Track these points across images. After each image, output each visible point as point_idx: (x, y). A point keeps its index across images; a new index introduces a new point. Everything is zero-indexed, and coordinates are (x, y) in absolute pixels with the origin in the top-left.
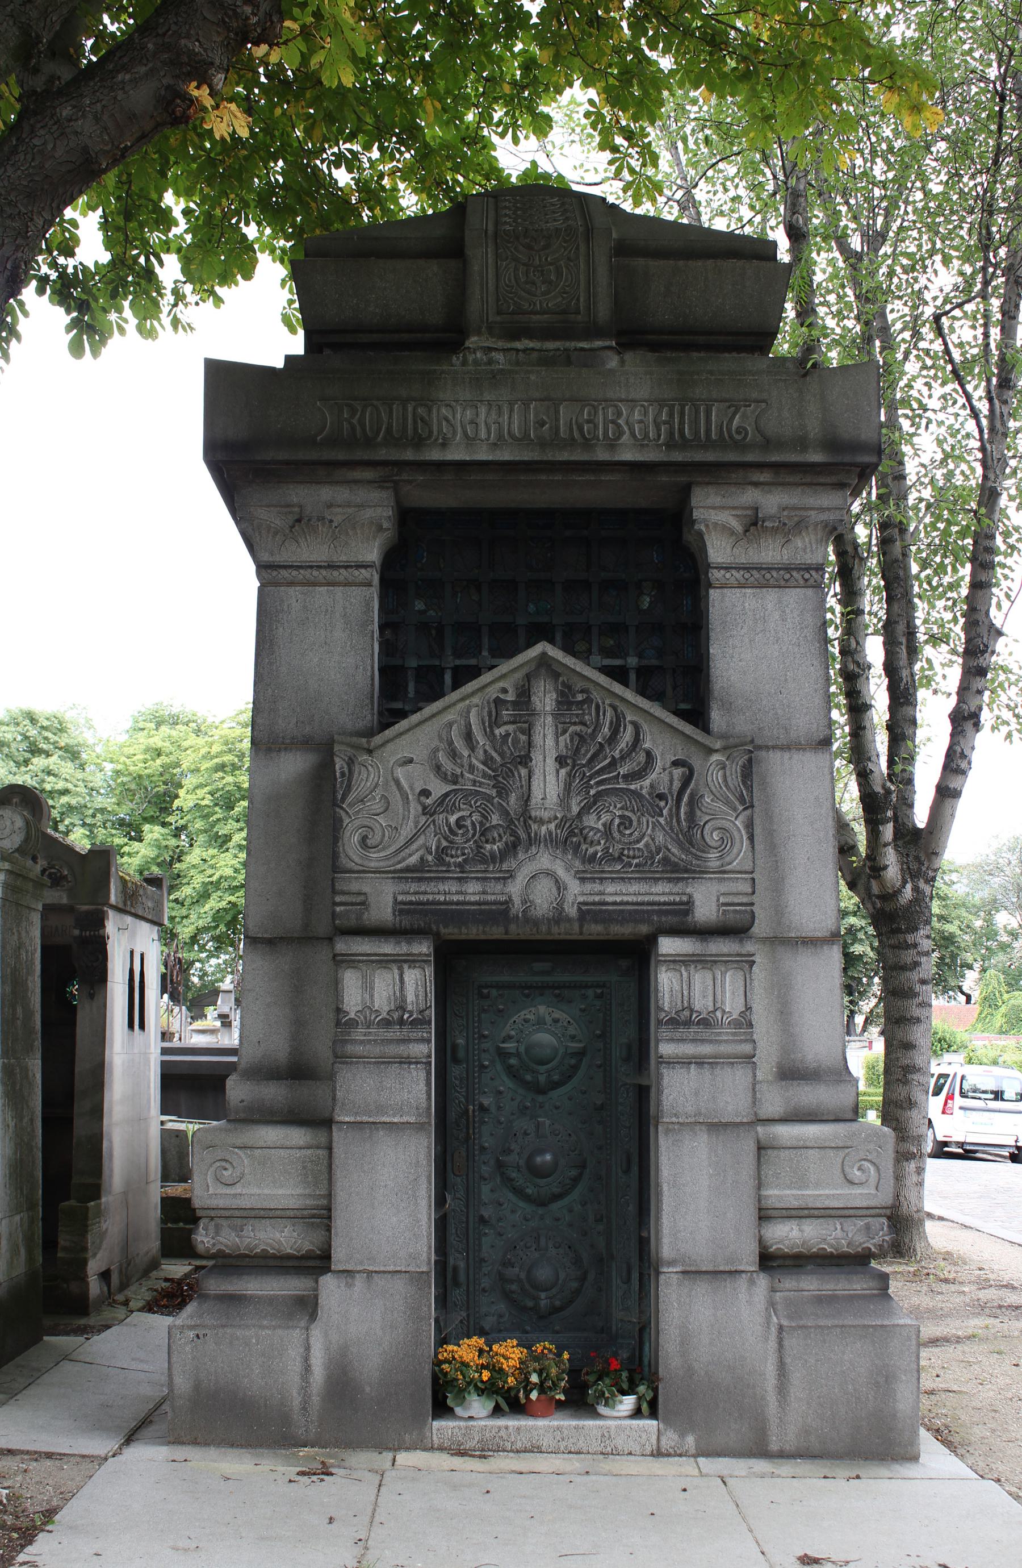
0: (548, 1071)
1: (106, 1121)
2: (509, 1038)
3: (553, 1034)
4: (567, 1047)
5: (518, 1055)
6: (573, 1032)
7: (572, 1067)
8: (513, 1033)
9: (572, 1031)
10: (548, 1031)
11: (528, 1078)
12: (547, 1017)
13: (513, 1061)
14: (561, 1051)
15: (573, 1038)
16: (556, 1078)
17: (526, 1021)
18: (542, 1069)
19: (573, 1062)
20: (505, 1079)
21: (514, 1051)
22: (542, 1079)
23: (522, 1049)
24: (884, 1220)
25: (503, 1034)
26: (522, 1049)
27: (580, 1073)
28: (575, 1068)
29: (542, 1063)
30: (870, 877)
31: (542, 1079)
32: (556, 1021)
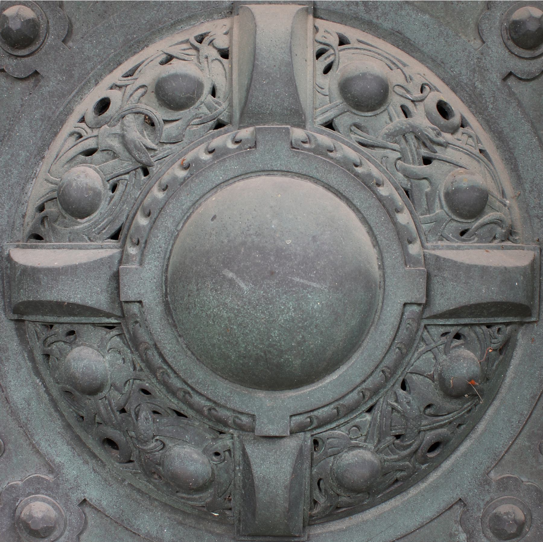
0: (309, 424)
1: (287, 391)
2: (72, 207)
3: (351, 184)
4: (432, 273)
5: (119, 319)
6: (473, 176)
7: (454, 393)
8: (88, 177)
9: (465, 165)
10: (314, 163)
11: (189, 458)
12: (308, 72)
13: (92, 357)
14: (400, 292)
15: (469, 208)
16: (359, 459)
17: (173, 97)
18: (272, 409)
19: (464, 362)
20: (61, 452)
21: (95, 295)
22: (274, 468)
23: (143, 283)
24: (53, 525)
25: (38, 190)
26: (143, 283)
27: (497, 423)
28: (470, 396)
29: (274, 376)
30: (257, 232)
31: (274, 468)
32: (364, 98)
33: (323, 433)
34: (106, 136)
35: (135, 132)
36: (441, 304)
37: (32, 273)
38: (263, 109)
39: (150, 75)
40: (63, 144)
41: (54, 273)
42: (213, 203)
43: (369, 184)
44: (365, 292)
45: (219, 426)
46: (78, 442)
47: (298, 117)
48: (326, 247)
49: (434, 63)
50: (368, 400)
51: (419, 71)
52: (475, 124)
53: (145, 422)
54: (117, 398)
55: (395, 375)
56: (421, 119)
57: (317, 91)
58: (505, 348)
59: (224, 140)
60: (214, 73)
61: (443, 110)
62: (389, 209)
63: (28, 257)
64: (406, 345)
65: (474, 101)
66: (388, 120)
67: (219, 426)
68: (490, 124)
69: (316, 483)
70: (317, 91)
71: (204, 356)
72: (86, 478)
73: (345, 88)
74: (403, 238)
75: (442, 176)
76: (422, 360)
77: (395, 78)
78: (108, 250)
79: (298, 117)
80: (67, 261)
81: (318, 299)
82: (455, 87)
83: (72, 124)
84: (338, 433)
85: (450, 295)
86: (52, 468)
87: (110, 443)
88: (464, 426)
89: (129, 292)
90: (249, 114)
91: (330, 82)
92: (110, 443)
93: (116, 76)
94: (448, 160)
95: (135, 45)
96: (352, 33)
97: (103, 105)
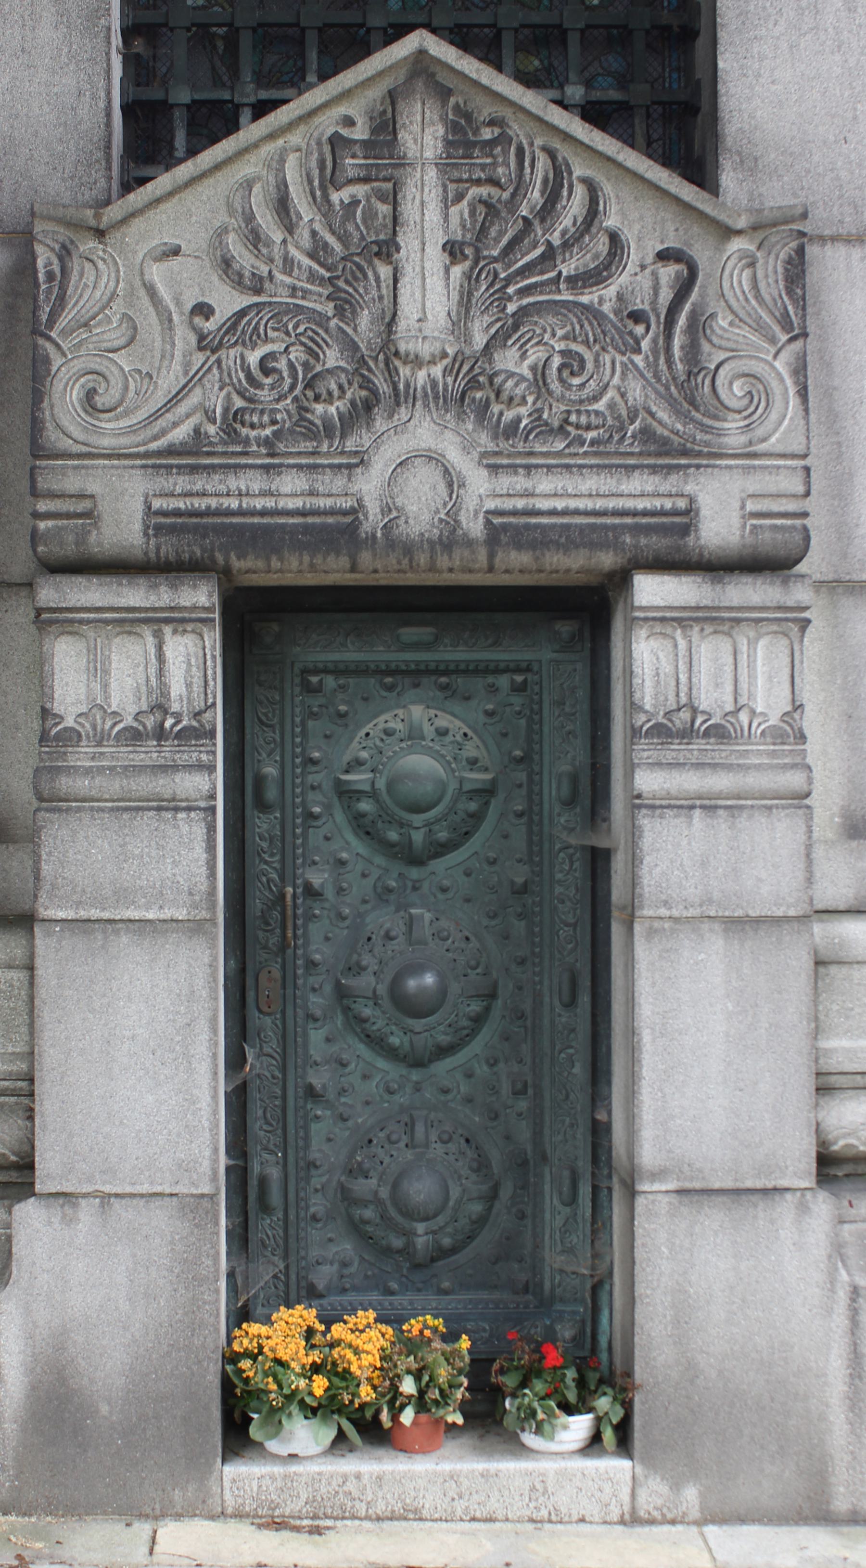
0: (428, 824)
3: (438, 757)
4: (461, 781)
5: (373, 794)
7: (472, 815)
8: (364, 755)
9: (471, 750)
10: (428, 751)
11: (393, 835)
13: (365, 806)
14: (453, 786)
15: (473, 763)
16: (443, 835)
17: (389, 733)
18: (418, 819)
19: (473, 806)
21: (367, 787)
22: (418, 837)
23: (381, 784)
26: (381, 784)
27: (486, 827)
28: (477, 818)
29: (417, 808)
31: (418, 837)
32: (442, 733)
33: (433, 827)
34: (370, 743)
35: (378, 743)
36: (465, 789)
37: (348, 782)
38: (414, 735)
39: (381, 726)
40: (355, 744)
41: (355, 782)
42: (401, 762)
43: (443, 756)
44: (442, 786)
45: (402, 825)
46: (356, 834)
47: (423, 738)
48: (845, 737)
49: (463, 721)
50: (444, 817)
51: (458, 723)
52: (475, 738)
53: (380, 825)
54: (371, 818)
55: (452, 810)
56: (459, 738)
57: (428, 730)
58: (487, 803)
59: (403, 745)
60: (399, 726)
61: (465, 735)
62: (449, 763)
63: (345, 777)
64: (455, 801)
65: (475, 731)
66: (449, 738)
67: (402, 825)
68: (480, 737)
69: (97, 367)
70: (428, 730)
71: (398, 804)
72: (358, 846)
73: (437, 730)
74: (453, 771)
75: (465, 754)
76: (461, 806)
77: (451, 726)
78: (371, 775)
79: (423, 738)
80: (359, 778)
81: (429, 787)
82: (470, 727)
83: (357, 739)
84: (436, 828)
85: (467, 787)
86: (347, 843)
87: (368, 833)
88: (476, 828)
89: (377, 786)
90: (410, 738)
91: (432, 729)
92: (368, 833)
93: (371, 725)
94: (695, 669)
95: (376, 716)
96: (439, 713)
97: (367, 734)
